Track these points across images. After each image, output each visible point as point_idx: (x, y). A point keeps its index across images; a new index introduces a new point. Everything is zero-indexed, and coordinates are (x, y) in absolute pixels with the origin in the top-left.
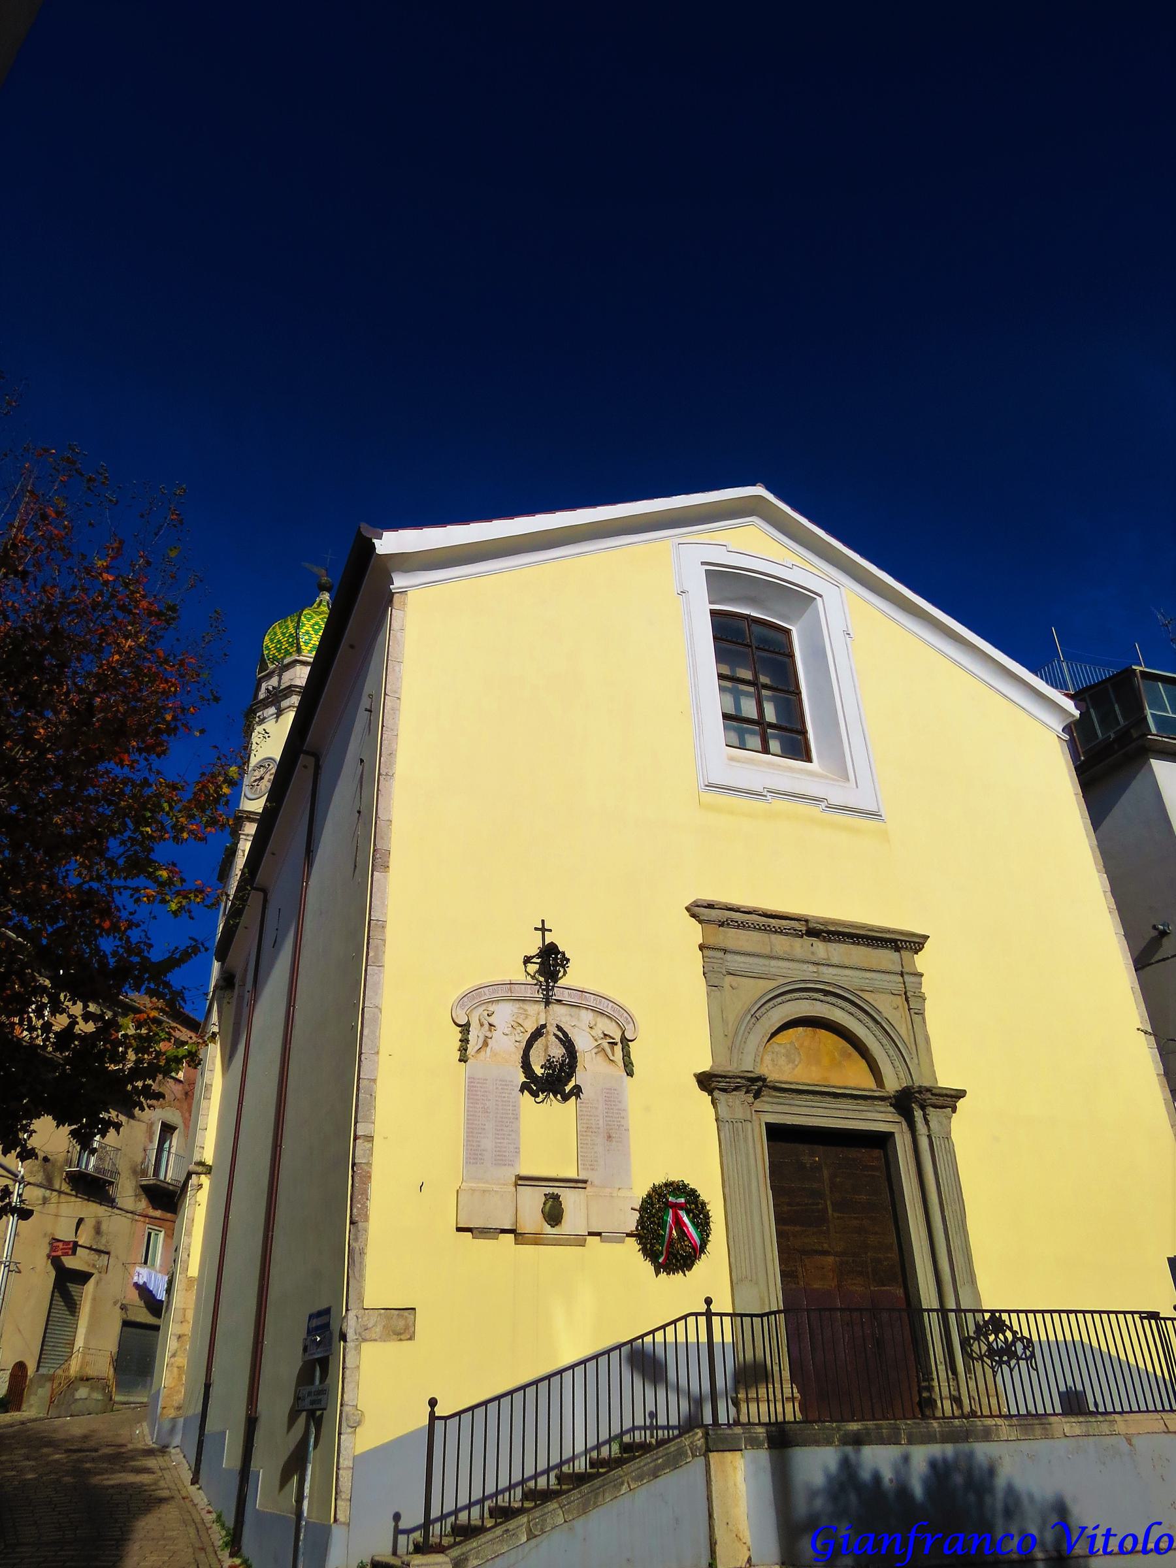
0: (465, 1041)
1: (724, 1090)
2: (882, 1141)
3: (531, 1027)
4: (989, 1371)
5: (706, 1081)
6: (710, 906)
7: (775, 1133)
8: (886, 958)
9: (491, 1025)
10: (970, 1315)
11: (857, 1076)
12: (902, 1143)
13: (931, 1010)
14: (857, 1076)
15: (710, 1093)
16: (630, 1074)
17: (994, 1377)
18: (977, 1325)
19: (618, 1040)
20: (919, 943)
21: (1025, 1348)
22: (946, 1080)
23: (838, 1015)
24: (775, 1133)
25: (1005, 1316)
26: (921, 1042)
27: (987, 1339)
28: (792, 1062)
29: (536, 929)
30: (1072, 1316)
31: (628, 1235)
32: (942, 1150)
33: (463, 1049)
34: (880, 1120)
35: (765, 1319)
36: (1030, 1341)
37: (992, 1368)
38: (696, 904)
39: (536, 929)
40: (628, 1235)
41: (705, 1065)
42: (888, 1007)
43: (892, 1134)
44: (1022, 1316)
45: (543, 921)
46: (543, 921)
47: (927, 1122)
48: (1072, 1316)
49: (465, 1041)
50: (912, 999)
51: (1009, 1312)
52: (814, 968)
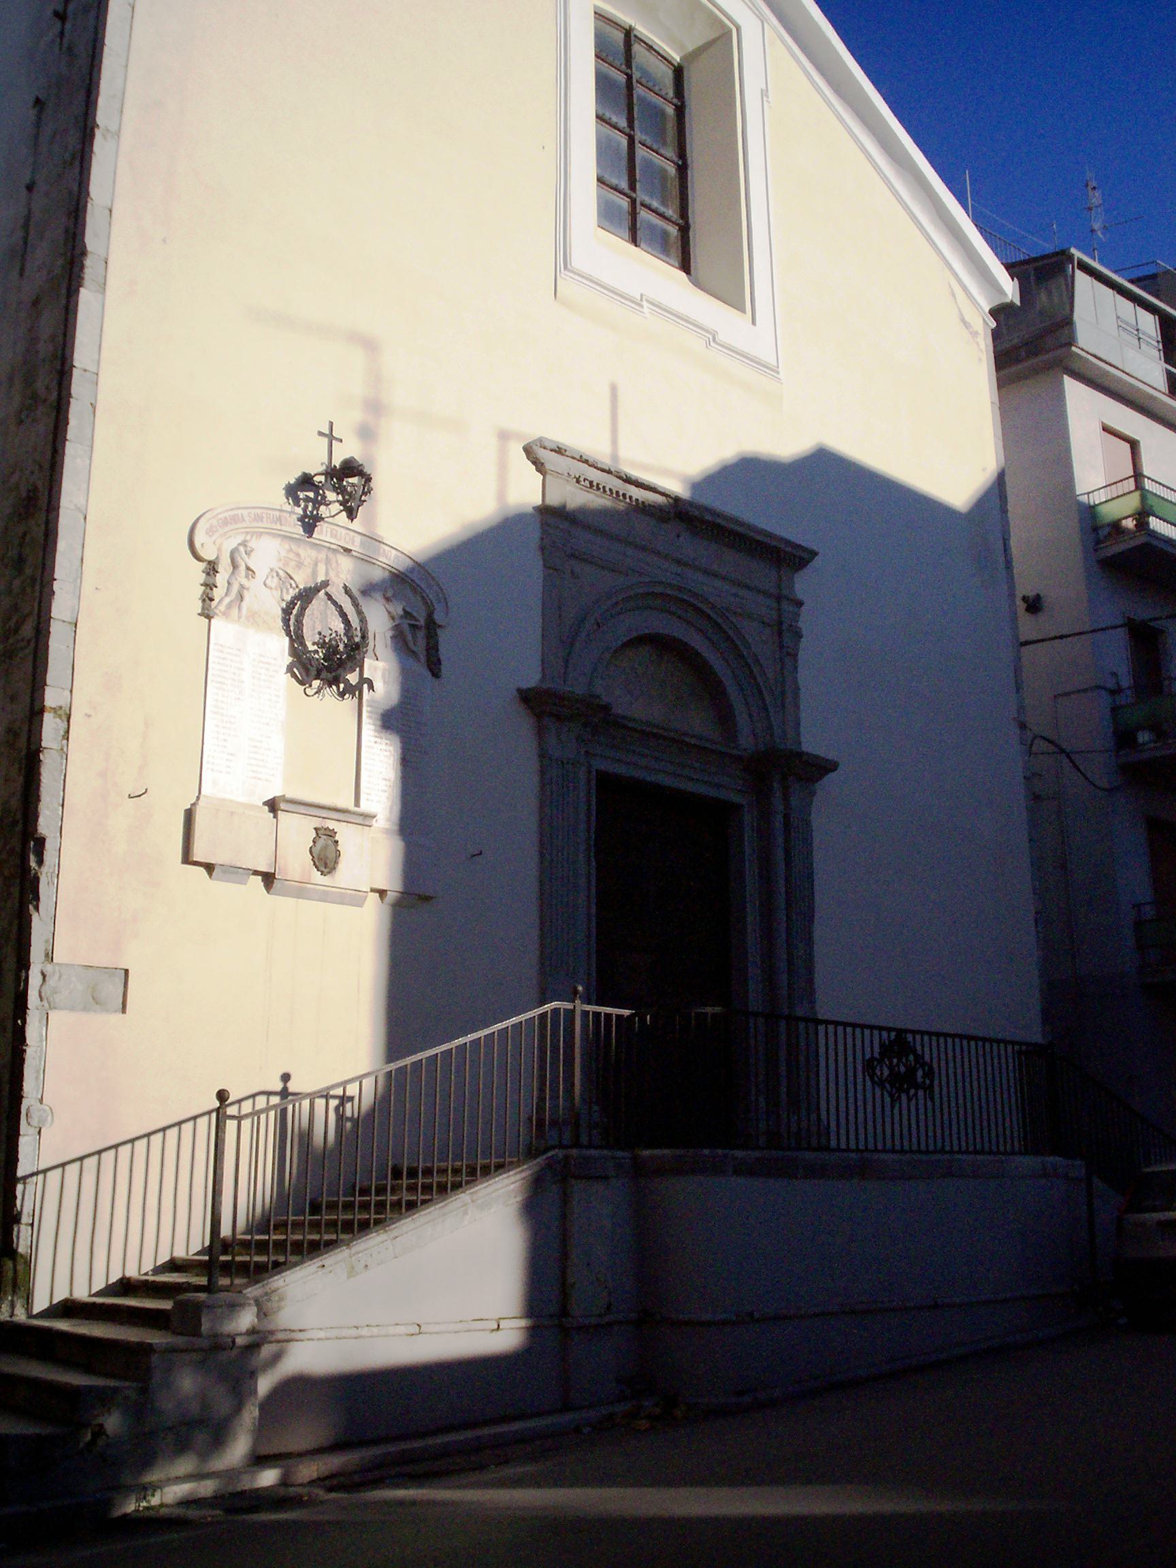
0: (209, 586)
1: (558, 717)
2: (723, 812)
3: (303, 580)
4: (888, 1100)
5: (527, 697)
6: (559, 451)
7: (607, 785)
8: (762, 574)
9: (248, 568)
10: (802, 1026)
11: (697, 722)
12: (749, 818)
13: (807, 651)
14: (697, 722)
15: (539, 716)
16: (436, 674)
17: (893, 1107)
18: (882, 1045)
19: (422, 622)
20: (801, 558)
21: (925, 1075)
22: (813, 742)
23: (697, 642)
24: (607, 785)
25: (910, 1038)
26: (784, 693)
27: (891, 1062)
28: (640, 696)
29: (321, 434)
30: (840, 1029)
31: (256, 873)
32: (797, 834)
33: (207, 599)
34: (728, 788)
35: (858, 1031)
36: (931, 1068)
37: (891, 1096)
38: (541, 443)
39: (321, 434)
40: (256, 873)
41: (531, 678)
42: (758, 640)
43: (742, 806)
44: (858, 1031)
45: (331, 424)
46: (331, 424)
47: (786, 798)
48: (840, 1029)
49: (209, 586)
50: (785, 634)
51: (914, 1032)
52: (675, 568)
